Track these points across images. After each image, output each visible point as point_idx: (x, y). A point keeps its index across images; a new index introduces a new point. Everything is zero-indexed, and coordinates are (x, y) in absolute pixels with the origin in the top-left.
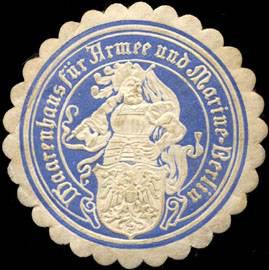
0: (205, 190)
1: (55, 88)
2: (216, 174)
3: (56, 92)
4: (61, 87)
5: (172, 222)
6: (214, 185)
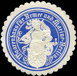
0: (58, 55)
1: (15, 26)
2: (61, 50)
3: (16, 28)
4: (17, 26)
5: (49, 64)
6: (61, 53)
